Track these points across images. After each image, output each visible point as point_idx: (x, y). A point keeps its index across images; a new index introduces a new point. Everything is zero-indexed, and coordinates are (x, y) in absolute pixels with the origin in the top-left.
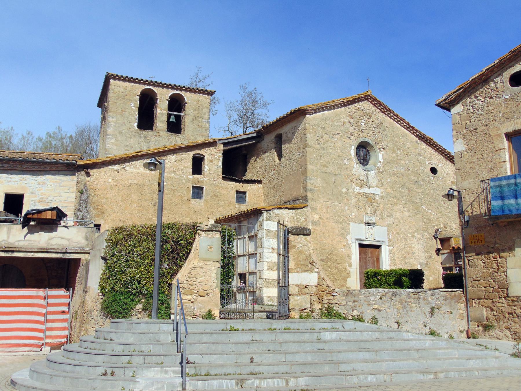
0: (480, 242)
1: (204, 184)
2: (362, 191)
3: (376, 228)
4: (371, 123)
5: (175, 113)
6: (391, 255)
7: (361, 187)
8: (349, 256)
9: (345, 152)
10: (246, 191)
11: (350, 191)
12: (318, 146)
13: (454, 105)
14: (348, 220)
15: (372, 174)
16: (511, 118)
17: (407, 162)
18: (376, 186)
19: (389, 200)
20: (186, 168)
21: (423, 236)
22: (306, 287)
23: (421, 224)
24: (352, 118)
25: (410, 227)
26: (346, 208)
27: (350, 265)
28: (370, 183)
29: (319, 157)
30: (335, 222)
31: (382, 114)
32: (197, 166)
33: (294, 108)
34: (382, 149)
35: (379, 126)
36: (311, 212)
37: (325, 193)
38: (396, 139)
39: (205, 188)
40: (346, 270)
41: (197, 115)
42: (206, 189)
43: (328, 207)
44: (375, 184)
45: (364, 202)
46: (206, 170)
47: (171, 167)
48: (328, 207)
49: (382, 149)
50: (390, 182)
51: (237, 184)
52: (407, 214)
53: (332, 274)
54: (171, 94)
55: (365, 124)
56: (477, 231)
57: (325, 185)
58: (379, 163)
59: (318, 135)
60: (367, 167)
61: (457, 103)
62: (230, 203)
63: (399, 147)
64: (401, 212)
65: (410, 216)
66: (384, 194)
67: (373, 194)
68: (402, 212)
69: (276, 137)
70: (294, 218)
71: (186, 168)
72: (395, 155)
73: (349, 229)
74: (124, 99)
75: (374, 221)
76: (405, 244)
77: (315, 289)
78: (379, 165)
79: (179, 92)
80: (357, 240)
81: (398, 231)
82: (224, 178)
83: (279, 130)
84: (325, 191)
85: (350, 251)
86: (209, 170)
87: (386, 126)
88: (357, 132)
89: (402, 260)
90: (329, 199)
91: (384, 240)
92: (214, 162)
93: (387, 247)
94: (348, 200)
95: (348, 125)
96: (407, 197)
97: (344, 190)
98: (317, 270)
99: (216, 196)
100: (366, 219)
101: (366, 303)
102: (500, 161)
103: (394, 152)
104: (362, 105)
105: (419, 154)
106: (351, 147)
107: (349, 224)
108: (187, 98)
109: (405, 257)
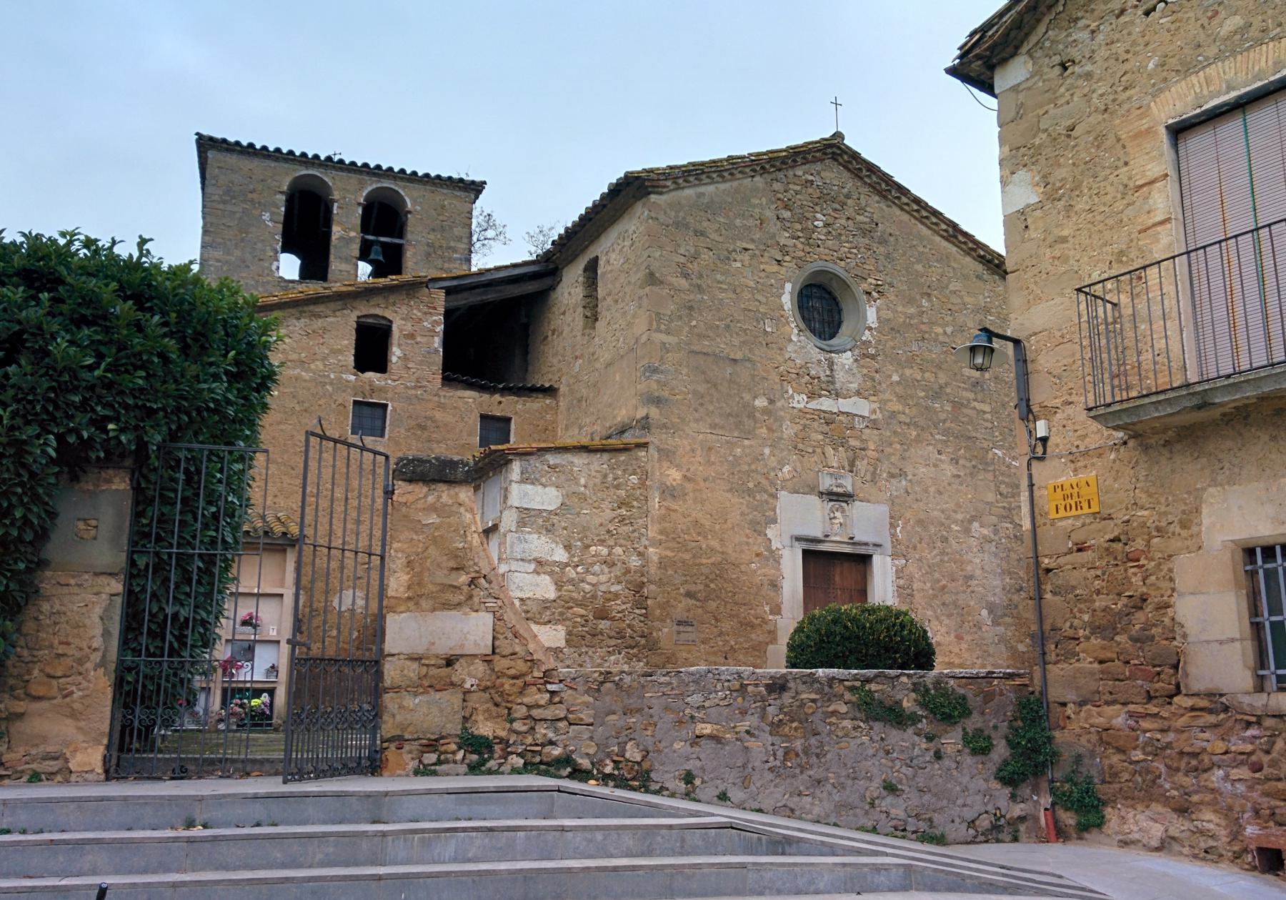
0: (1085, 505)
1: (389, 395)
2: (813, 405)
3: (857, 510)
4: (843, 221)
5: (382, 239)
6: (901, 582)
7: (812, 396)
8: (775, 585)
9: (764, 300)
10: (509, 415)
11: (779, 404)
12: (684, 283)
13: (1004, 61)
14: (773, 484)
15: (846, 359)
16: (1187, 69)
17: (949, 330)
18: (858, 393)
19: (895, 432)
20: (335, 352)
21: (996, 532)
22: (449, 662)
23: (991, 497)
24: (786, 207)
25: (958, 505)
26: (767, 451)
27: (777, 610)
28: (838, 386)
29: (684, 312)
30: (730, 490)
31: (877, 198)
32: (372, 349)
33: (615, 176)
34: (874, 294)
35: (865, 233)
36: (660, 460)
37: (701, 410)
38: (919, 267)
39: (390, 408)
40: (765, 622)
41: (437, 244)
42: (394, 409)
43: (710, 449)
44: (854, 386)
45: (821, 437)
46: (394, 359)
47: (293, 350)
48: (710, 449)
49: (874, 294)
50: (898, 383)
51: (486, 397)
52: (949, 470)
53: (721, 634)
54: (370, 189)
55: (827, 225)
56: (1075, 470)
57: (702, 388)
58: (867, 332)
59: (682, 252)
60: (834, 341)
61: (1014, 55)
62: (463, 446)
63: (925, 289)
64: (931, 466)
65: (959, 476)
66: (879, 416)
67: (848, 414)
68: (935, 466)
69: (585, 270)
70: (605, 476)
71: (335, 352)
72: (912, 310)
73: (774, 510)
74: (244, 201)
75: (850, 489)
76: (943, 553)
77: (480, 667)
78: (867, 336)
79: (387, 184)
80: (798, 539)
81: (922, 516)
82: (447, 380)
83: (591, 248)
84: (702, 405)
85: (779, 570)
86: (405, 358)
87: (889, 230)
88: (800, 246)
89: (935, 596)
90: (714, 426)
91: (878, 541)
92: (419, 339)
93: (889, 559)
94: (770, 429)
95: (773, 227)
96: (947, 425)
97: (761, 402)
98: (491, 603)
99: (423, 428)
100: (826, 483)
101: (671, 717)
102: (1150, 222)
103: (911, 301)
104: (819, 173)
105: (987, 310)
106: (783, 287)
107: (775, 497)
108: (414, 201)
109: (944, 587)
